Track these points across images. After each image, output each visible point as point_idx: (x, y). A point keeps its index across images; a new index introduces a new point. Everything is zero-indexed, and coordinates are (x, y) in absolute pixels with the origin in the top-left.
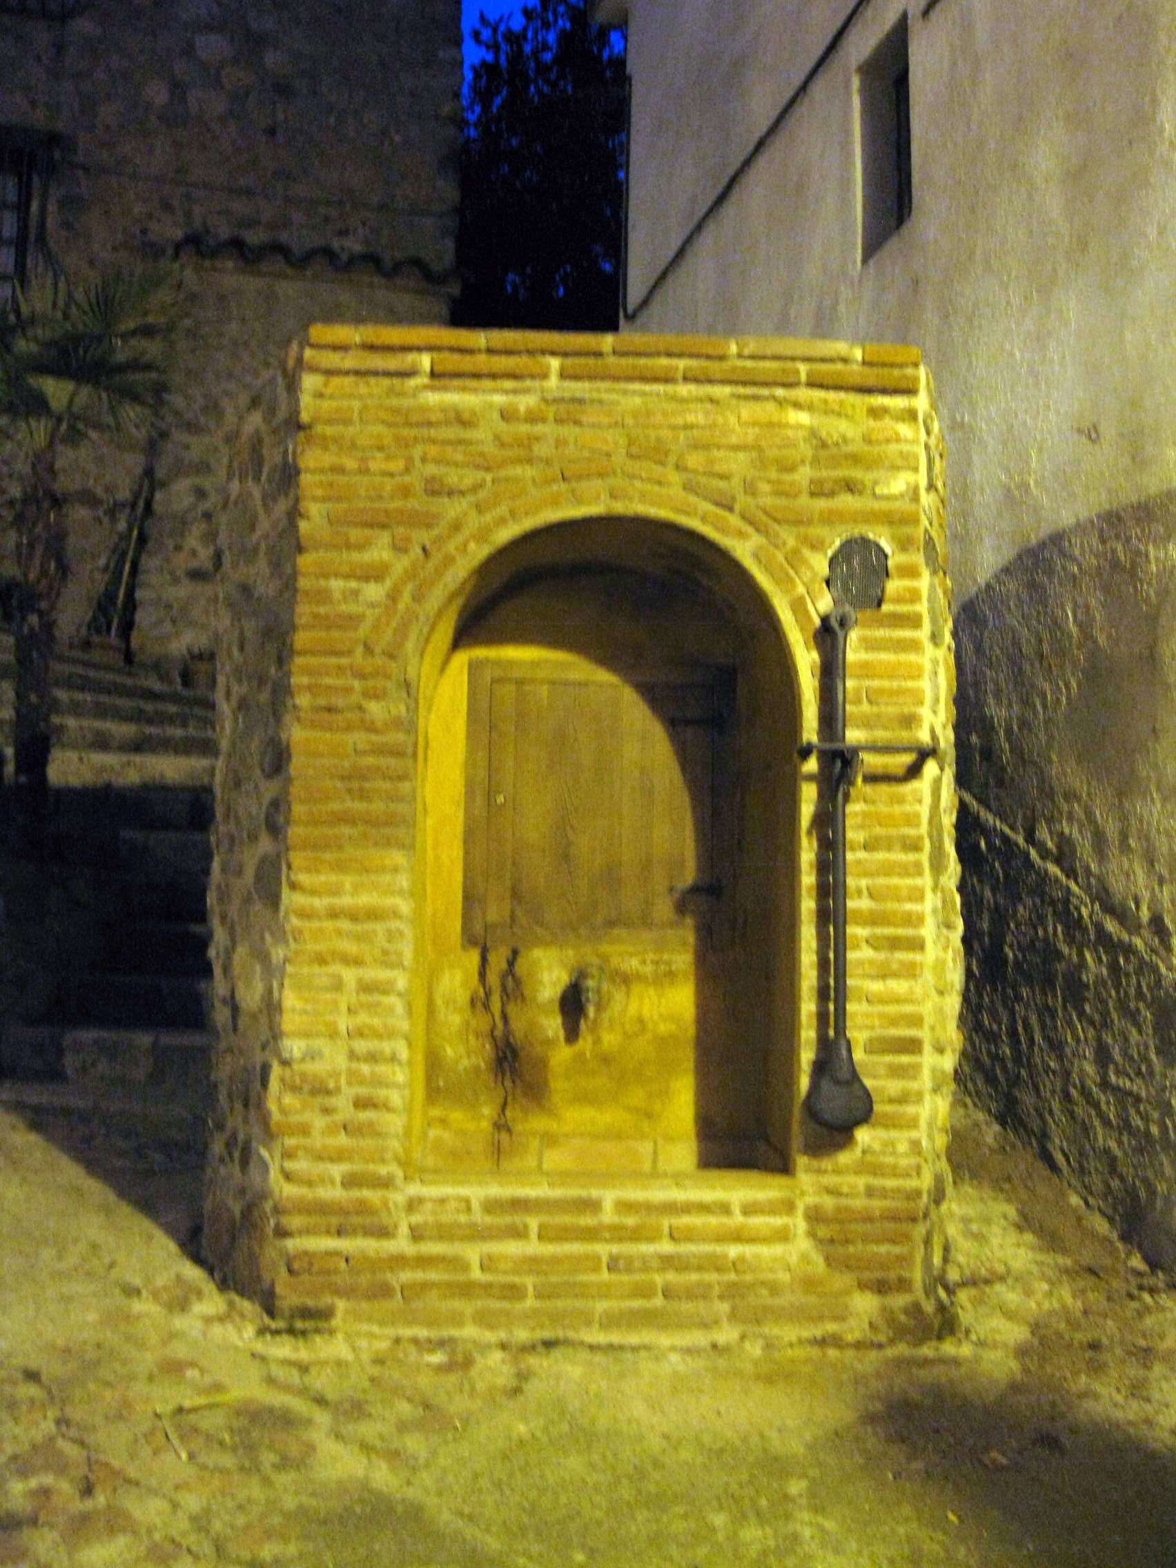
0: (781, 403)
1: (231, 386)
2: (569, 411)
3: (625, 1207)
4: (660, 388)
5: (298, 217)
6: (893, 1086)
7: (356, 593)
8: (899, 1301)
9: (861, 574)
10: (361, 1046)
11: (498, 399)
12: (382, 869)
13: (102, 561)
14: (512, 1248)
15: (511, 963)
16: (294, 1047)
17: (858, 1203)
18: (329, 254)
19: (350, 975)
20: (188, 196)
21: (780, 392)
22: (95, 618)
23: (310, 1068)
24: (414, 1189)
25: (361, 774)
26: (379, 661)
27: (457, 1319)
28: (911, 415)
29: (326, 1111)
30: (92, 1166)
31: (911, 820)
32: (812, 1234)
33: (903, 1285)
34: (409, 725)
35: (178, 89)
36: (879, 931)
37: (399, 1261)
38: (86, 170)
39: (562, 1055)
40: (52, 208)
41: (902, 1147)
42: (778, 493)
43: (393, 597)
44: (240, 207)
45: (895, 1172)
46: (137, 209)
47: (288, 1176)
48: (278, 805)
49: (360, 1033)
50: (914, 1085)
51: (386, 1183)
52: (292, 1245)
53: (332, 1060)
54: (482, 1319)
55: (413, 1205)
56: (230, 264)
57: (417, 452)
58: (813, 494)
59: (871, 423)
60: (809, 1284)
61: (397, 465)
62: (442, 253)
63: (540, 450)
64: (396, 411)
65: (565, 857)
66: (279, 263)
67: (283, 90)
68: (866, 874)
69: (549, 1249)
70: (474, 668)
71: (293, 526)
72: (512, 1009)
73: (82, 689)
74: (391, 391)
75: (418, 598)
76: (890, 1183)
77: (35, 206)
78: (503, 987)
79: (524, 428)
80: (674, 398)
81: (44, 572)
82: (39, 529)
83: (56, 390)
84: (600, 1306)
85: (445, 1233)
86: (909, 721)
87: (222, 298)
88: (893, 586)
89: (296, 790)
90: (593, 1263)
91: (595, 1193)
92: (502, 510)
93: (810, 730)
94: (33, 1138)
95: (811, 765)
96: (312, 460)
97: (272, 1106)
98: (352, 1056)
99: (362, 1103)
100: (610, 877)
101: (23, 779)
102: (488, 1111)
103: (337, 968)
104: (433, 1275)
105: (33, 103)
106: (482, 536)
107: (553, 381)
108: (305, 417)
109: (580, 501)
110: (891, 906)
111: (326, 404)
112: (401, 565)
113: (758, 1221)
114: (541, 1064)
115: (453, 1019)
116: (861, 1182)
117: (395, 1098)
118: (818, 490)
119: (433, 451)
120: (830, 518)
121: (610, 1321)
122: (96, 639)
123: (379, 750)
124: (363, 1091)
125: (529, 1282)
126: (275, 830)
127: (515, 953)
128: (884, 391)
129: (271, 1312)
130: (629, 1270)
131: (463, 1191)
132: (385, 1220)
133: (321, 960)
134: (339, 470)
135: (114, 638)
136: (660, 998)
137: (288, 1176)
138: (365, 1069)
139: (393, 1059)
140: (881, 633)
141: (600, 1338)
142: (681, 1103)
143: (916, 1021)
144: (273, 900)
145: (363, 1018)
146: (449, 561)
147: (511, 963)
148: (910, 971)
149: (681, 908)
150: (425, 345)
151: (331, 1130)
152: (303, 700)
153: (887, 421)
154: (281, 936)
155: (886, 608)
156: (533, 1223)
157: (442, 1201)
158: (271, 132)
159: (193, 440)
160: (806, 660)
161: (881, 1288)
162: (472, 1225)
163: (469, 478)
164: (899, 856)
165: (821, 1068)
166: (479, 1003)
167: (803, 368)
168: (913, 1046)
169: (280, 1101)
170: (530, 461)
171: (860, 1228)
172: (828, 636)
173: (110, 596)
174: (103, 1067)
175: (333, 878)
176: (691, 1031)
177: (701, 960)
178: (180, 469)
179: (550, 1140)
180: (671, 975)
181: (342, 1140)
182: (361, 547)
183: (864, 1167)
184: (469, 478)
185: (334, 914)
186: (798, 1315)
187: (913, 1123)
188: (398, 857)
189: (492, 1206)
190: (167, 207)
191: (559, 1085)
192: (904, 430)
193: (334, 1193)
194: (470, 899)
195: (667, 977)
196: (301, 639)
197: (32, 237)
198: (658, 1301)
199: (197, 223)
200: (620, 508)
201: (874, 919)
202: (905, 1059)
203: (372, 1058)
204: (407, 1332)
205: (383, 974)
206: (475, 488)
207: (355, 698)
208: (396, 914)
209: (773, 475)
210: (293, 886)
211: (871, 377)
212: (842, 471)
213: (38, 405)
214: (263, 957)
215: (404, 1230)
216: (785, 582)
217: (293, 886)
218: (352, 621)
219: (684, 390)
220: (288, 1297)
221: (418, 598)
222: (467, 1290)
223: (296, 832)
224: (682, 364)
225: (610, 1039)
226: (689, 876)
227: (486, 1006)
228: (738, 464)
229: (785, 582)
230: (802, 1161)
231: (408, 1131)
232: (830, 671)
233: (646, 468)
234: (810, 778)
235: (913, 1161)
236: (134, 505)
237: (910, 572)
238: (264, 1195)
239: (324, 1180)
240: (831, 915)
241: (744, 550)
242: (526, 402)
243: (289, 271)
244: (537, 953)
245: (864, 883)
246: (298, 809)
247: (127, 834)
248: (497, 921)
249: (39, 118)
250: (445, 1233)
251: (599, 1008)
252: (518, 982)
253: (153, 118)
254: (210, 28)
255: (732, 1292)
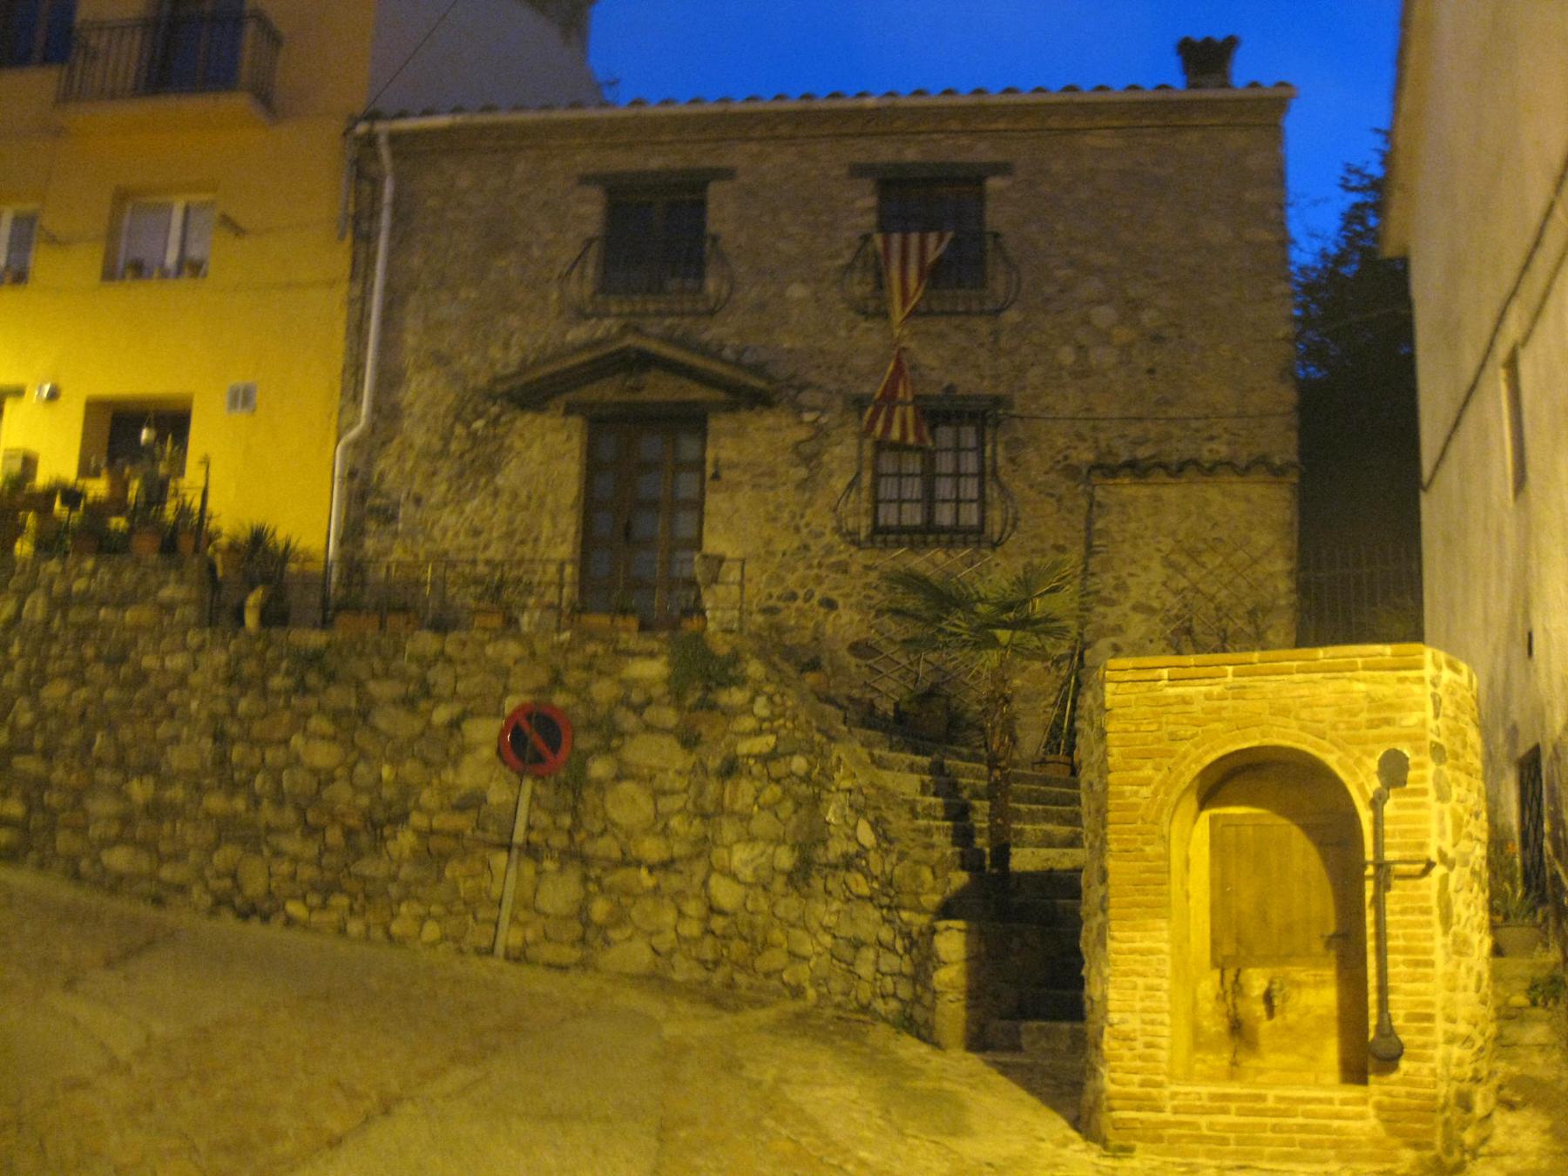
0: (1350, 679)
1: (1133, 569)
2: (1239, 693)
3: (1280, 1099)
4: (1285, 677)
5: (1176, 431)
6: (1420, 1039)
7: (1136, 793)
8: (1429, 1154)
9: (1394, 770)
10: (1148, 1017)
11: (1203, 689)
12: (1154, 929)
13: (1052, 699)
14: (1222, 1119)
15: (1237, 976)
16: (1114, 1017)
17: (1403, 1101)
18: (1195, 463)
19: (1140, 981)
20: (1094, 428)
21: (1349, 674)
22: (1048, 743)
23: (1123, 1027)
24: (1175, 1088)
25: (1145, 883)
26: (1148, 826)
27: (1195, 1155)
28: (1421, 680)
29: (1131, 1049)
30: (1032, 1091)
31: (1425, 898)
32: (1377, 1116)
33: (1430, 1146)
34: (1166, 857)
35: (1080, 348)
36: (1411, 957)
37: (1168, 1124)
38: (1022, 418)
39: (1265, 1025)
40: (1000, 449)
41: (1425, 1071)
42: (1349, 729)
43: (1155, 794)
44: (1134, 431)
45: (1421, 1084)
46: (1060, 442)
47: (1113, 1081)
48: (1104, 898)
49: (1144, 1011)
50: (1431, 1039)
51: (1159, 1085)
52: (1117, 1114)
53: (1133, 1024)
54: (1210, 1154)
55: (1174, 1096)
56: (1127, 481)
57: (1164, 719)
58: (1369, 728)
59: (1399, 686)
60: (1377, 1143)
61: (1153, 727)
62: (1283, 445)
63: (1225, 714)
64: (1153, 699)
65: (1264, 918)
66: (1161, 476)
67: (1157, 339)
68: (1401, 927)
69: (1243, 1120)
70: (1213, 819)
71: (1104, 760)
72: (1238, 1001)
73: (1037, 802)
74: (1150, 690)
75: (1167, 794)
76: (1420, 1091)
77: (988, 449)
78: (1234, 989)
79: (1217, 703)
80: (1292, 682)
81: (1002, 744)
82: (997, 717)
83: (1003, 635)
84: (1268, 1150)
85: (1189, 1110)
86: (1422, 846)
87: (1123, 505)
88: (1411, 774)
89: (1112, 891)
90: (1263, 1127)
91: (1263, 1092)
92: (1207, 747)
93: (1369, 856)
94: (1001, 1078)
95: (1370, 871)
96: (1112, 727)
97: (1105, 1047)
98: (1144, 1022)
99: (1149, 1045)
100: (1289, 929)
101: (995, 871)
102: (1227, 1055)
103: (1135, 979)
104: (1183, 1131)
105: (982, 377)
106: (1198, 760)
107: (1230, 678)
108: (1108, 705)
109: (1245, 740)
110: (1414, 944)
111: (1118, 698)
112: (1159, 777)
113: (1348, 1108)
114: (1254, 1031)
115: (1207, 1007)
116: (1403, 1090)
117: (1164, 1042)
118: (1372, 724)
119: (1172, 718)
120: (1379, 740)
121: (1273, 1158)
122: (1050, 758)
123: (1150, 870)
124: (1149, 1039)
125: (1232, 1136)
126: (1104, 911)
127: (1239, 971)
128: (1405, 668)
129: (1106, 1148)
130: (1281, 1132)
131: (1197, 1089)
132: (1161, 1104)
133: (1126, 974)
134: (1126, 731)
135: (1062, 756)
136: (1318, 996)
137: (1113, 1081)
138: (1149, 1028)
139: (1162, 1023)
140: (1407, 799)
141: (1268, 1166)
142: (1331, 1052)
143: (1430, 1004)
144: (1104, 946)
145: (1147, 1003)
146: (1182, 774)
147: (1237, 976)
148: (1426, 978)
149: (1328, 945)
150: (1163, 666)
151: (1134, 1058)
152: (1113, 847)
153: (1408, 685)
154: (1107, 961)
155: (1408, 786)
156: (1233, 1106)
157: (1187, 1094)
158: (1151, 371)
159: (1108, 610)
160: (1366, 816)
161: (1417, 1146)
162: (1202, 1107)
163: (1191, 731)
164: (1422, 918)
165: (1379, 1027)
166: (1221, 998)
167: (1359, 661)
168: (1429, 1018)
169: (1109, 1044)
170: (1219, 720)
171: (1405, 1114)
172: (1376, 803)
173: (1057, 725)
174: (1043, 1043)
175: (1130, 934)
176: (1335, 1013)
177: (1340, 975)
178: (1101, 633)
179: (1260, 1071)
180: (1323, 982)
181: (1138, 1063)
182: (1138, 769)
183: (1404, 1082)
184: (1191, 731)
185: (1132, 952)
186: (1370, 1158)
187: (1431, 1059)
188: (1162, 924)
189: (1213, 1097)
190: (1080, 437)
191: (1264, 1042)
192: (1417, 689)
193: (1135, 1090)
194: (1215, 944)
195: (1319, 984)
196: (1111, 816)
197: (988, 470)
198: (1298, 1149)
199: (1103, 444)
200: (1267, 742)
201: (1407, 950)
202: (1426, 1024)
203: (1152, 1022)
204: (1170, 1159)
205: (1157, 981)
206: (1193, 736)
207: (1139, 845)
208: (1161, 952)
209: (1346, 718)
210: (1112, 938)
211: (1397, 661)
212: (1383, 712)
213: (994, 643)
214: (1100, 973)
215: (1168, 1108)
216: (1354, 774)
217: (1112, 938)
218: (1135, 807)
219: (1298, 677)
220: (1114, 1141)
221: (1167, 794)
222: (1200, 1139)
223: (1111, 912)
224: (1295, 664)
225: (1291, 1017)
226: (1332, 929)
227: (1224, 999)
228: (1327, 715)
229: (1354, 774)
230: (1372, 1078)
231: (1171, 1061)
232: (1378, 822)
233: (1280, 720)
234: (1370, 877)
235: (1431, 1079)
236: (1072, 657)
237: (1421, 766)
238: (1102, 1091)
239: (1130, 1083)
240: (1381, 951)
241: (1331, 760)
242: (1217, 690)
243: (1169, 480)
244: (1250, 971)
245: (1400, 932)
246: (1113, 900)
247: (1060, 902)
248: (1232, 952)
249: (986, 387)
250: (1189, 1110)
251: (1284, 1000)
252: (1241, 987)
253: (1064, 373)
254: (1100, 303)
255: (1336, 1145)
